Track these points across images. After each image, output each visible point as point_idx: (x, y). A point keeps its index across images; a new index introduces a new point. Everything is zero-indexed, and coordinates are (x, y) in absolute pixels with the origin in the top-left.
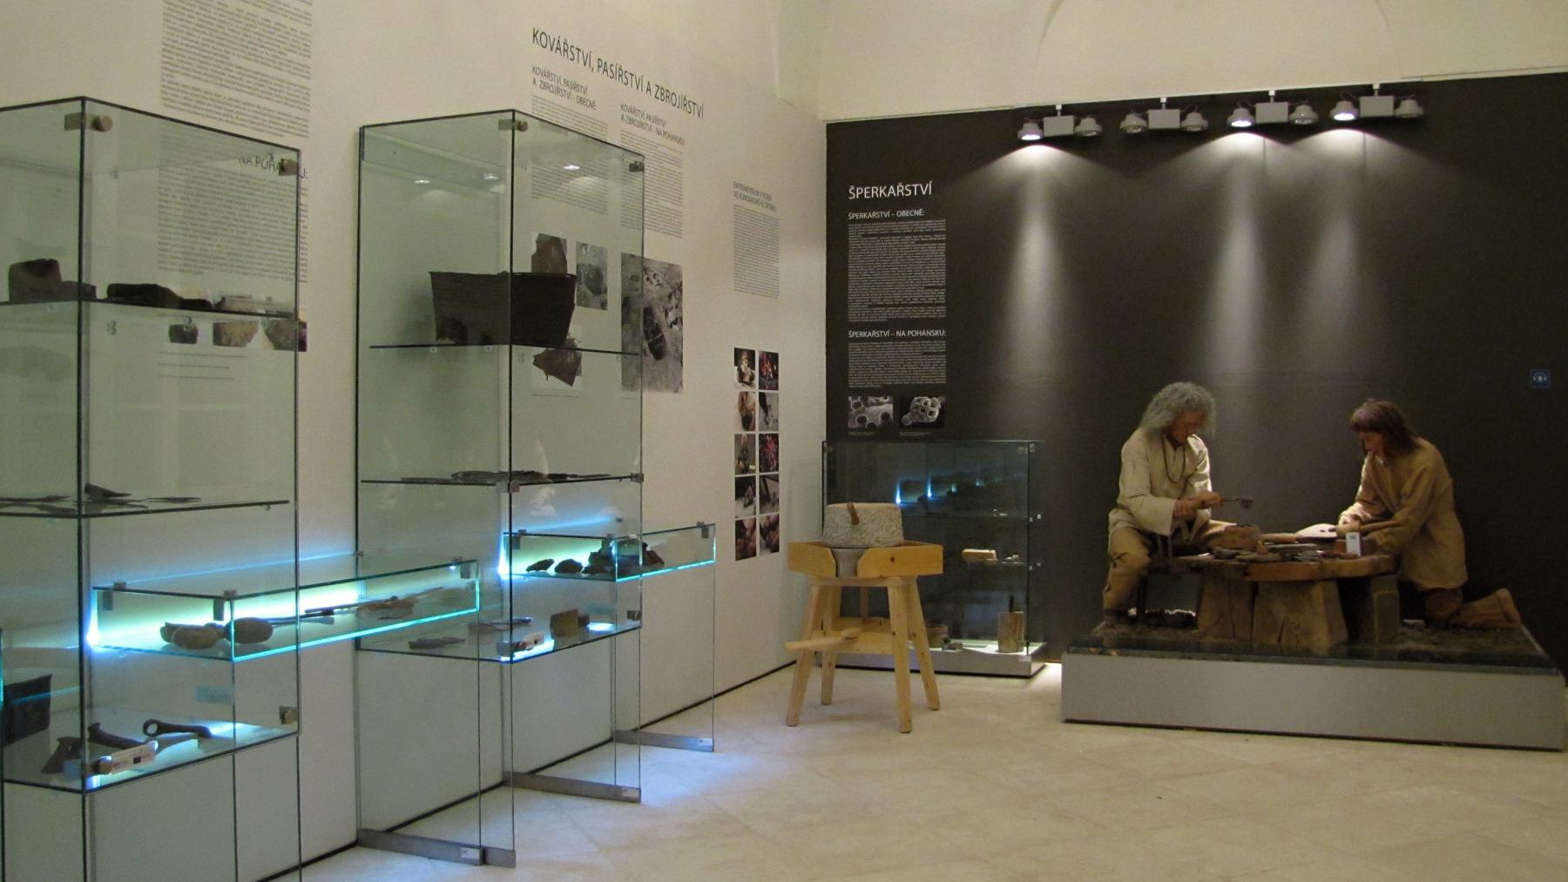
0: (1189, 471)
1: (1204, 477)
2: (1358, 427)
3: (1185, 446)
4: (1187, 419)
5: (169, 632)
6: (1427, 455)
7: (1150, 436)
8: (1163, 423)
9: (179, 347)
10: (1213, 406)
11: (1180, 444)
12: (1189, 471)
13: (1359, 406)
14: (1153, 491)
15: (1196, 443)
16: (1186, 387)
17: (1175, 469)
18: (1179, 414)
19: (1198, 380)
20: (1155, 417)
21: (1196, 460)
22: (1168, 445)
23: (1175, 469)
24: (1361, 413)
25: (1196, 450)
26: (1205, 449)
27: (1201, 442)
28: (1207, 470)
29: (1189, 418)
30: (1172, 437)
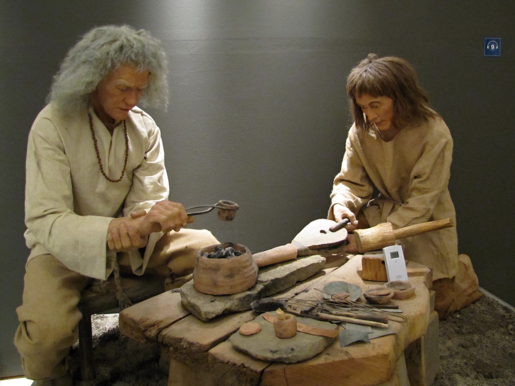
0: (134, 161)
1: (158, 168)
2: (362, 89)
3: (126, 124)
4: (124, 81)
5: (364, 261)
6: (440, 131)
7: (66, 116)
8: (81, 88)
9: (228, 222)
10: (165, 63)
11: (117, 123)
12: (134, 161)
13: (355, 64)
14: (79, 207)
15: (142, 121)
16: (125, 32)
17: (113, 163)
18: (108, 72)
19: (155, 34)
20: (72, 78)
21: (144, 146)
22: (100, 127)
23: (113, 163)
24: (362, 72)
25: (144, 131)
26: (157, 129)
27: (149, 120)
28: (160, 158)
29: (124, 80)
30: (102, 109)
